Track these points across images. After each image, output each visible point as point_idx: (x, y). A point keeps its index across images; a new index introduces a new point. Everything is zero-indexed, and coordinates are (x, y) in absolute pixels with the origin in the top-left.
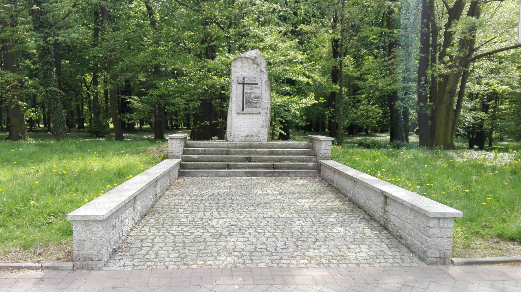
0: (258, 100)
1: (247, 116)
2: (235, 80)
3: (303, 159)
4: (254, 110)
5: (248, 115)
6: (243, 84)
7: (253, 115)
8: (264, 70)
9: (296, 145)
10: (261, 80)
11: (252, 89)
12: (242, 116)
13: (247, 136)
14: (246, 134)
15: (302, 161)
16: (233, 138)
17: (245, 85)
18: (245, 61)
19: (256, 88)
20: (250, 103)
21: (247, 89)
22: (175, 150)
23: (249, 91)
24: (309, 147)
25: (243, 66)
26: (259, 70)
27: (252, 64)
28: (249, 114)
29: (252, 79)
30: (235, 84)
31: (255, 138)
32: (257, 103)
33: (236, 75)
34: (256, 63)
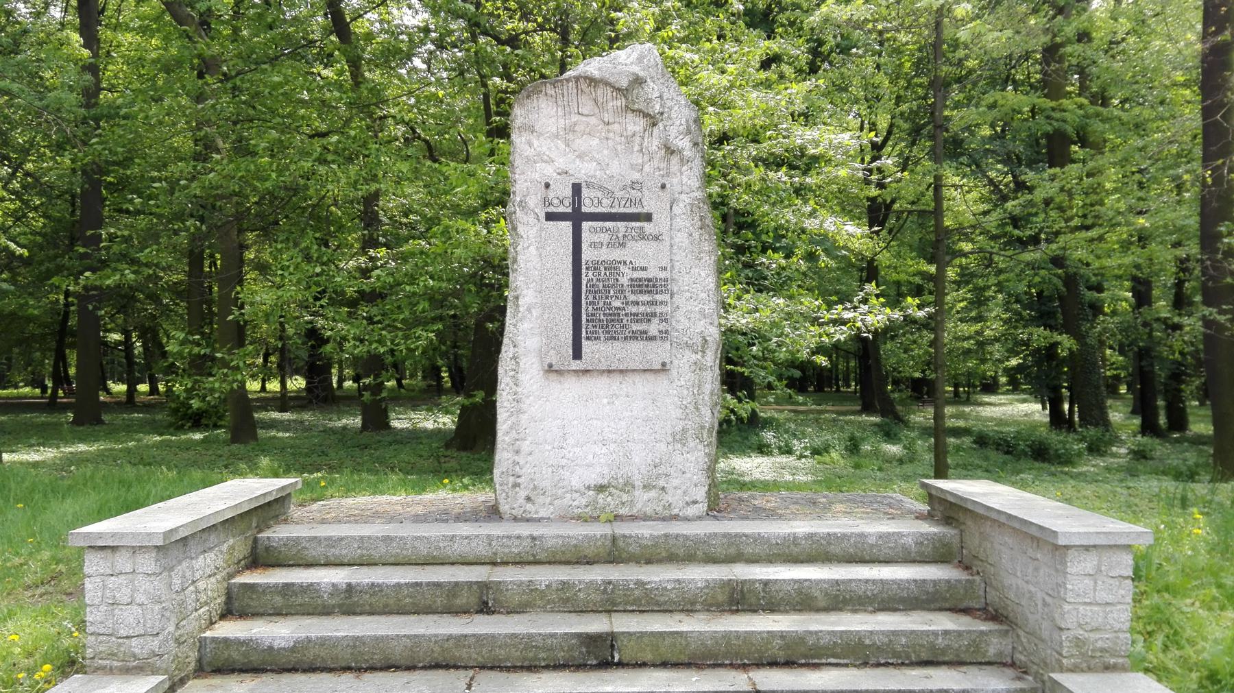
0: (653, 303)
1: (600, 385)
2: (533, 201)
3: (933, 647)
4: (630, 354)
5: (604, 380)
6: (577, 217)
7: (630, 378)
8: (684, 144)
9: (872, 540)
10: (665, 196)
11: (623, 245)
12: (572, 388)
13: (601, 488)
14: (593, 478)
15: (924, 656)
16: (528, 499)
17: (586, 225)
18: (584, 99)
19: (643, 236)
20: (614, 316)
21: (594, 245)
22: (129, 619)
23: (605, 254)
24: (940, 554)
25: (572, 129)
26: (654, 144)
27: (616, 112)
28: (610, 371)
29: (619, 194)
30: (531, 219)
31: (643, 500)
32: (648, 318)
33: (537, 176)
34: (641, 106)
